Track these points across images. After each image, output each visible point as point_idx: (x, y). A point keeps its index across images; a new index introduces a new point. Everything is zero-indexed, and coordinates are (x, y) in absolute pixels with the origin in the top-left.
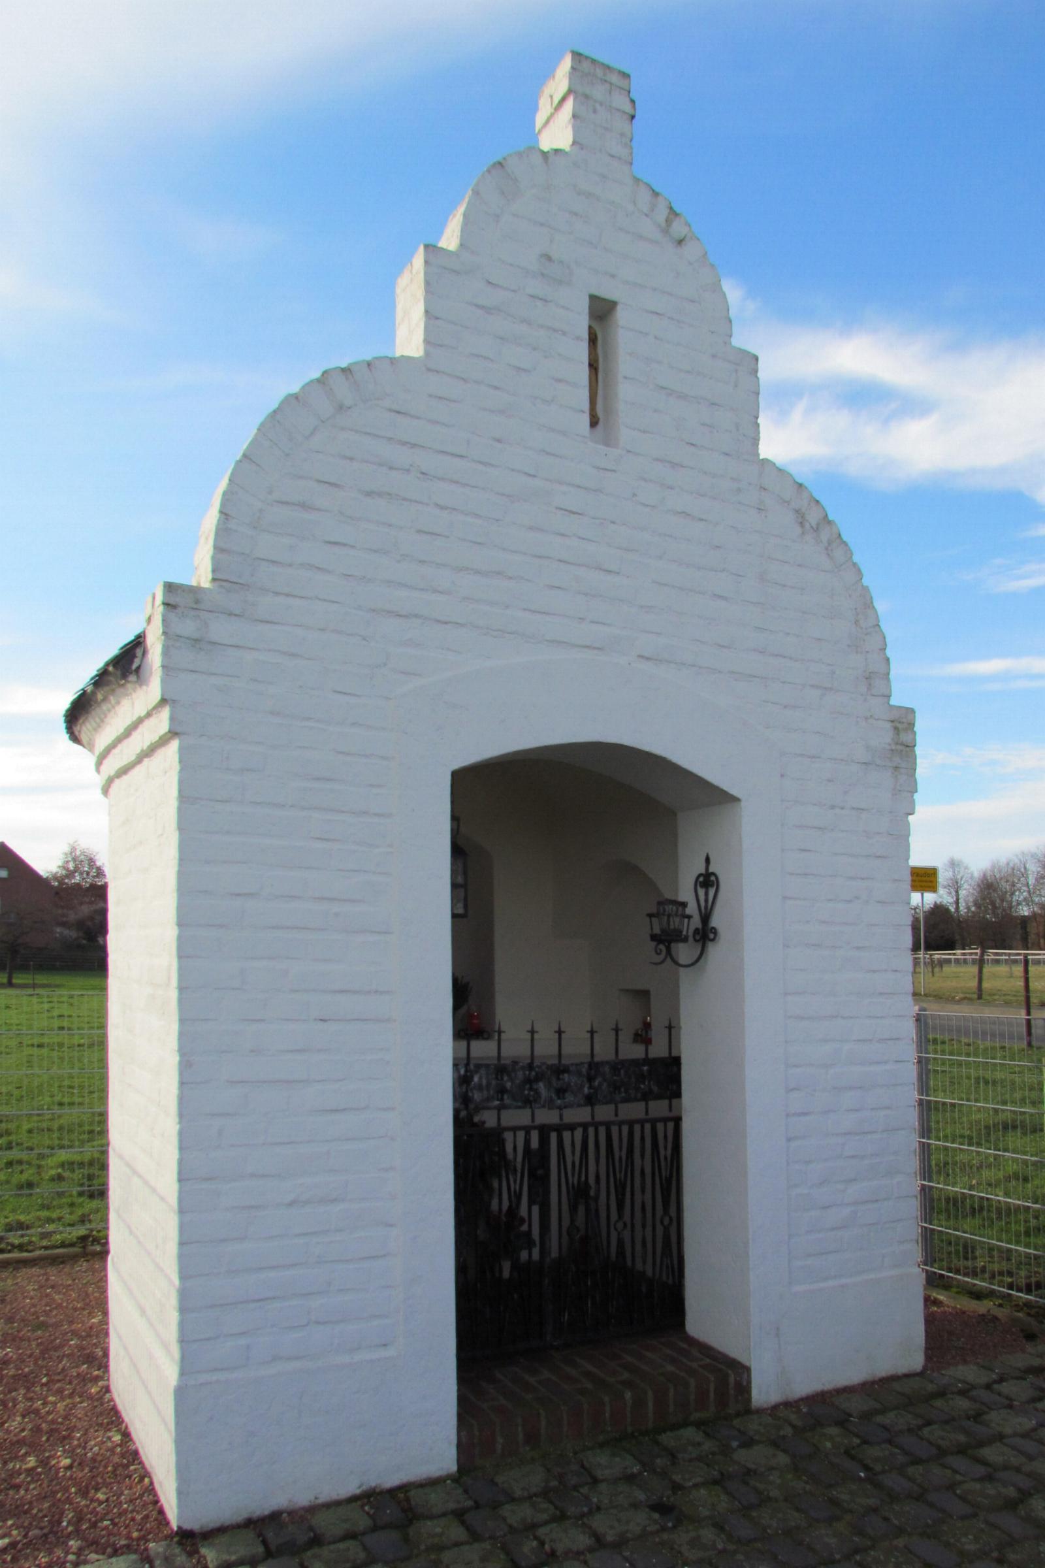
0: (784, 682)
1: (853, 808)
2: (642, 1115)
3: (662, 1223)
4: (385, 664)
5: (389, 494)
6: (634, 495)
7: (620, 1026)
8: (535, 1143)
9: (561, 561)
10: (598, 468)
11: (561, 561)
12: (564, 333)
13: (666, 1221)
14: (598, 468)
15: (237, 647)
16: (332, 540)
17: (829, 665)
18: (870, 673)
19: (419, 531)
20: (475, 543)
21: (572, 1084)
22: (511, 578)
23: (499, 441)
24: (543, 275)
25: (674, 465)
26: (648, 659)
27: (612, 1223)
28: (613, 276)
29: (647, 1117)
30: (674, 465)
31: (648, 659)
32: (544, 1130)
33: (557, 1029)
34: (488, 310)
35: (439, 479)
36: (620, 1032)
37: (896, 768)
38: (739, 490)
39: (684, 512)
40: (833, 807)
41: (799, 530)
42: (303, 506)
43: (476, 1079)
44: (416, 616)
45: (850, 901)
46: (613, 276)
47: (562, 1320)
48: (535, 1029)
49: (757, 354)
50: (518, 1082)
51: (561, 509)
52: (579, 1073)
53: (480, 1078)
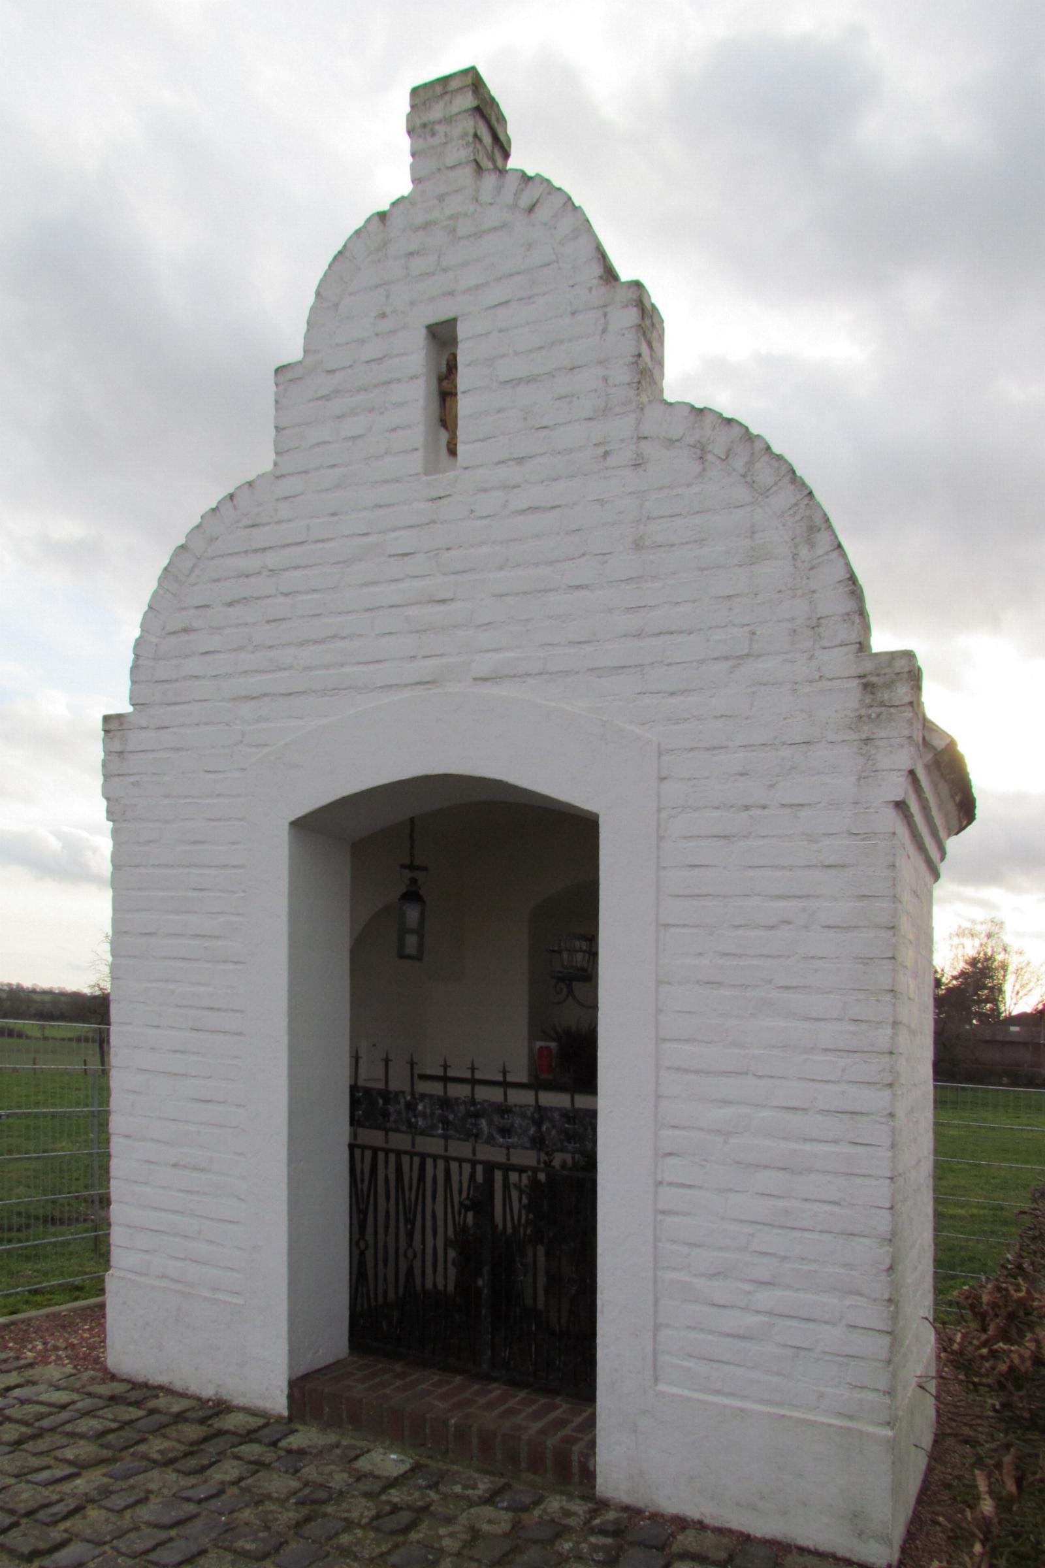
0: (669, 665)
1: (783, 805)
2: (408, 1148)
3: (406, 1255)
4: (241, 742)
5: (245, 598)
6: (472, 511)
7: (391, 1057)
8: (480, 1178)
9: (392, 606)
10: (432, 500)
11: (392, 606)
12: (398, 381)
13: (410, 1253)
14: (432, 500)
15: (143, 751)
16: (204, 651)
17: (744, 625)
18: (819, 619)
19: (268, 622)
20: (313, 616)
21: (516, 1125)
22: (345, 638)
23: (334, 514)
24: (377, 335)
25: (520, 461)
26: (485, 679)
27: (401, 1252)
28: (452, 293)
29: (474, 1158)
30: (520, 461)
31: (485, 679)
32: (490, 1167)
33: (443, 1063)
34: (326, 398)
35: (284, 570)
36: (390, 1063)
37: (867, 740)
38: (606, 454)
39: (530, 508)
40: (747, 808)
41: (696, 467)
42: (186, 630)
43: (420, 1107)
44: (265, 695)
45: (772, 928)
46: (452, 293)
47: (503, 1355)
48: (448, 1063)
49: (634, 278)
50: (460, 1115)
51: (394, 555)
52: (524, 1116)
53: (425, 1107)
